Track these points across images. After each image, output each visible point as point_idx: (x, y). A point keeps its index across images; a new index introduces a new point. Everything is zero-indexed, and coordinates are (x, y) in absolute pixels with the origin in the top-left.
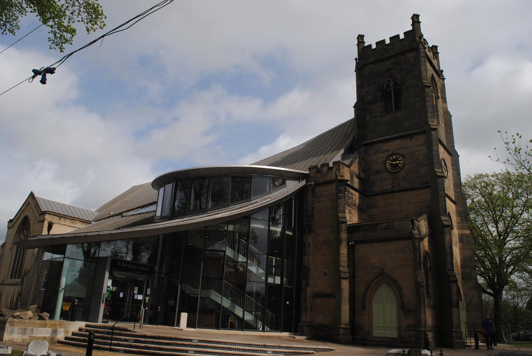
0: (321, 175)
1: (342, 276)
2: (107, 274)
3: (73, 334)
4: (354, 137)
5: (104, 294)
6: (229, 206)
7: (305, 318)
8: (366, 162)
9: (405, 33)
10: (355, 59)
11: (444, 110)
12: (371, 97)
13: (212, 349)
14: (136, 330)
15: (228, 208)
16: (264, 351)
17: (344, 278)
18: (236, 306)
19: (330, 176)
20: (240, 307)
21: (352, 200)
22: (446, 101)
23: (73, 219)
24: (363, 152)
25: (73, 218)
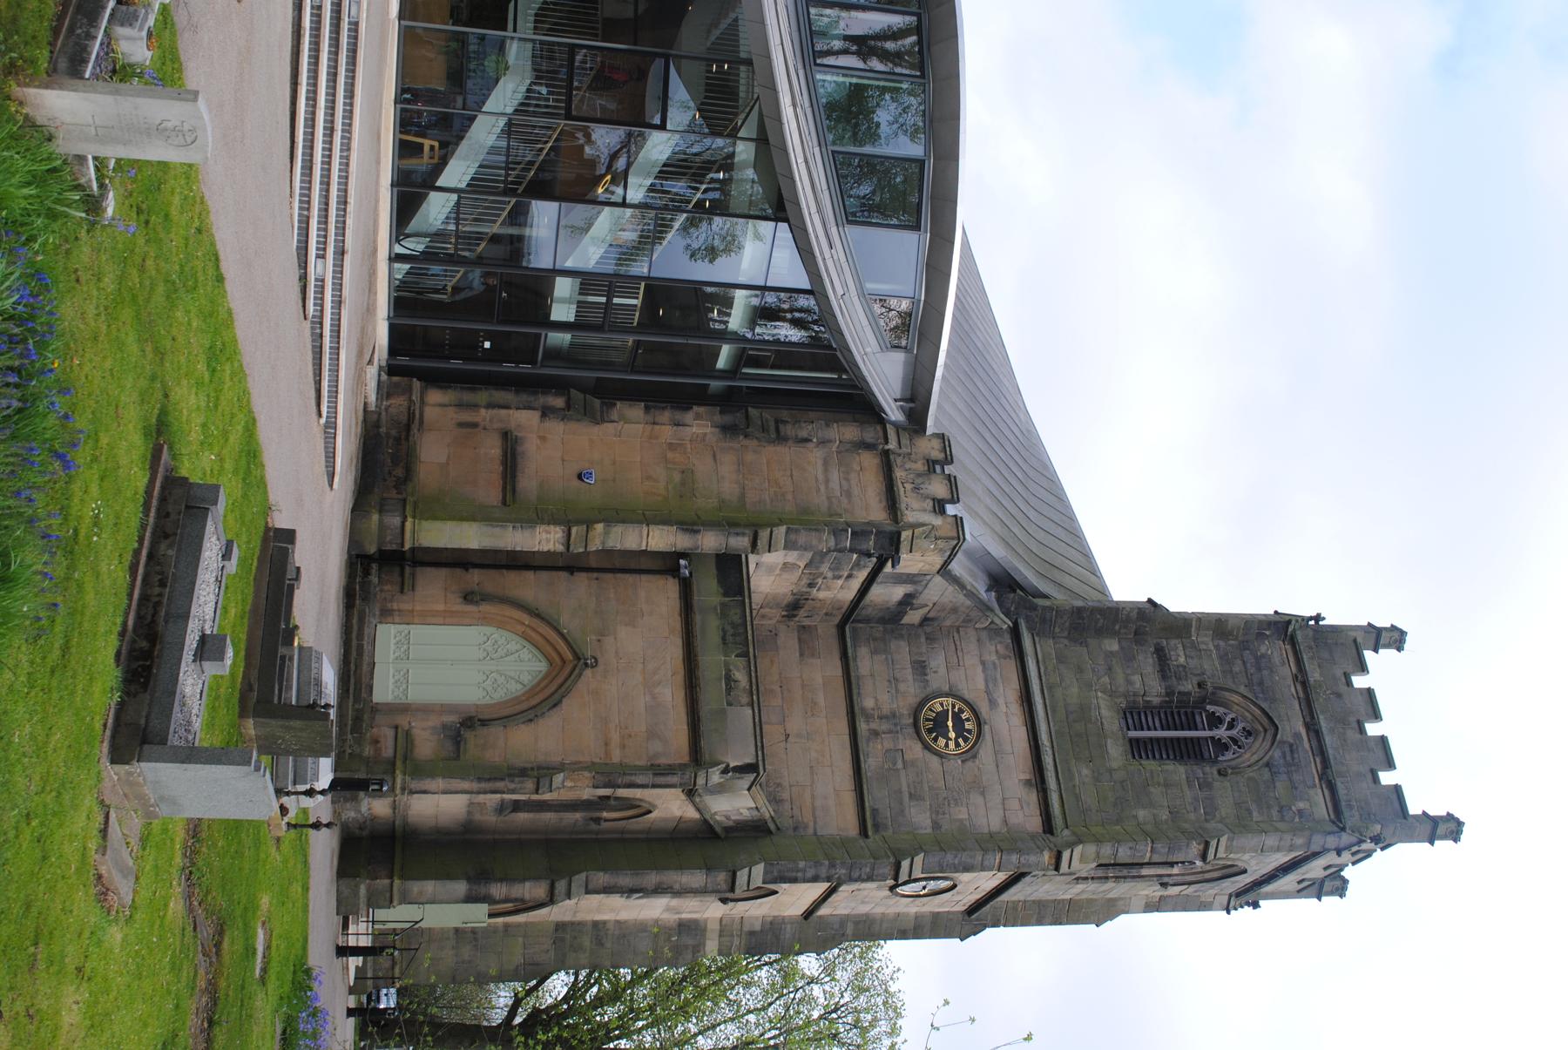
0: (919, 475)
1: (574, 530)
4: (1045, 596)
7: (437, 404)
8: (958, 632)
9: (1397, 789)
12: (1182, 660)
16: (325, 249)
19: (915, 504)
21: (830, 575)
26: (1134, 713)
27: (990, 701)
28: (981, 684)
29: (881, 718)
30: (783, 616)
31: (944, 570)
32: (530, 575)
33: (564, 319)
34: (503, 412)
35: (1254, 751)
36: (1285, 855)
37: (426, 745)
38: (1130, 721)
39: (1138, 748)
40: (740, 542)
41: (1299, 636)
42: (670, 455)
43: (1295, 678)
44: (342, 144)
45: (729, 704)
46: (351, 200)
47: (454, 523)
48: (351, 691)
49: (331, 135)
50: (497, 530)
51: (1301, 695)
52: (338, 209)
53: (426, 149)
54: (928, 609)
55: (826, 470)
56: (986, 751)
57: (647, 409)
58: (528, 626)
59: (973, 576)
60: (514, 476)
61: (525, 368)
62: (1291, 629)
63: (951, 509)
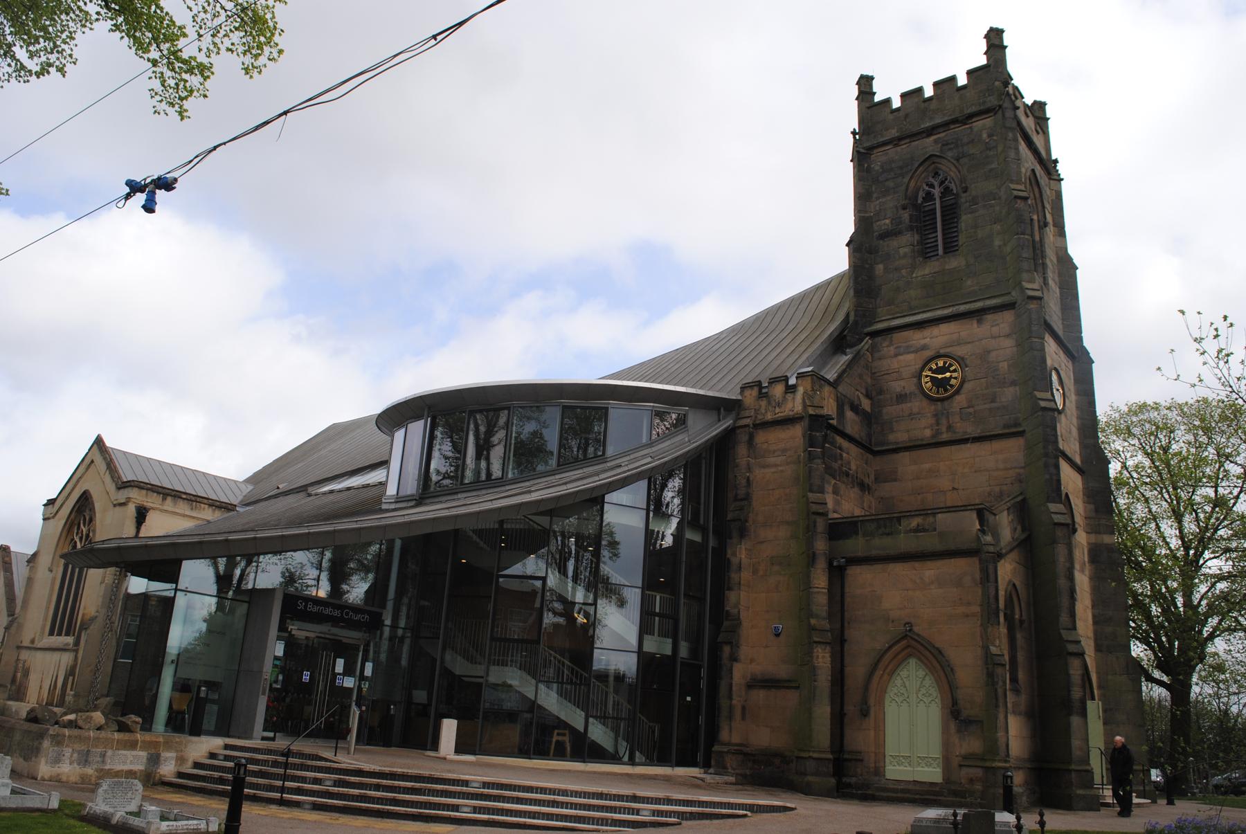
0: (769, 403)
2: (274, 631)
3: (197, 765)
4: (848, 315)
7: (731, 734)
8: (875, 373)
12: (887, 221)
19: (790, 405)
20: (578, 707)
26: (925, 252)
27: (922, 350)
28: (910, 357)
29: (938, 424)
30: (869, 493)
32: (847, 670)
35: (949, 170)
37: (973, 744)
39: (951, 247)
40: (821, 525)
41: (867, 144)
42: (761, 573)
43: (896, 145)
45: (935, 529)
46: (600, 790)
51: (908, 141)
53: (560, 738)
55: (768, 466)
56: (960, 351)
57: (730, 589)
58: (884, 671)
60: (779, 681)
61: (703, 673)
63: (792, 381)
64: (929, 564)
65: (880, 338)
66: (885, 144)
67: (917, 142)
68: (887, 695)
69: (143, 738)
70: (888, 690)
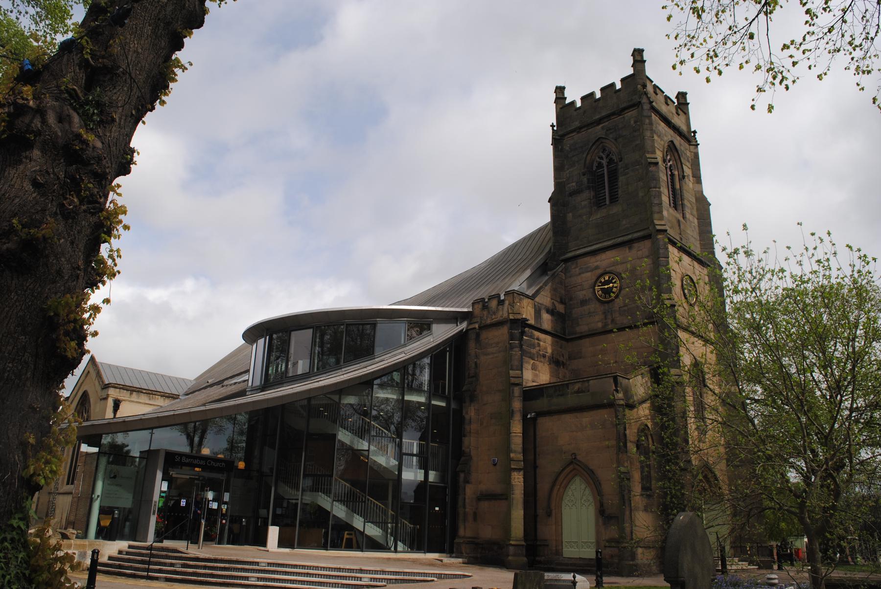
0: (489, 312)
2: (159, 475)
3: (110, 558)
4: (551, 249)
5: (155, 502)
6: (341, 369)
7: (465, 531)
9: (623, 80)
10: (551, 126)
11: (697, 195)
12: (574, 184)
13: (283, 575)
14: (189, 551)
15: (340, 370)
16: (358, 577)
17: (515, 469)
18: (355, 514)
19: (501, 313)
20: (361, 516)
21: (538, 348)
22: (701, 180)
23: (151, 393)
24: (561, 271)
25: (150, 392)
26: (599, 203)
28: (589, 274)
29: (606, 319)
30: (563, 367)
31: (532, 298)
32: (538, 486)
33: (423, 475)
34: (467, 501)
35: (611, 146)
36: (659, 124)
37: (612, 532)
38: (603, 204)
39: (614, 199)
40: (517, 391)
41: (560, 133)
43: (578, 132)
44: (316, 570)
45: (589, 391)
46: (338, 566)
47: (512, 522)
48: (589, 568)
49: (310, 574)
50: (515, 502)
51: (585, 129)
52: (343, 572)
53: (348, 536)
54: (555, 302)
56: (619, 268)
58: (560, 486)
59: (540, 283)
62: (557, 137)
64: (585, 414)
65: (570, 263)
66: (572, 131)
67: (591, 130)
68: (563, 502)
69: (75, 543)
70: (564, 499)
